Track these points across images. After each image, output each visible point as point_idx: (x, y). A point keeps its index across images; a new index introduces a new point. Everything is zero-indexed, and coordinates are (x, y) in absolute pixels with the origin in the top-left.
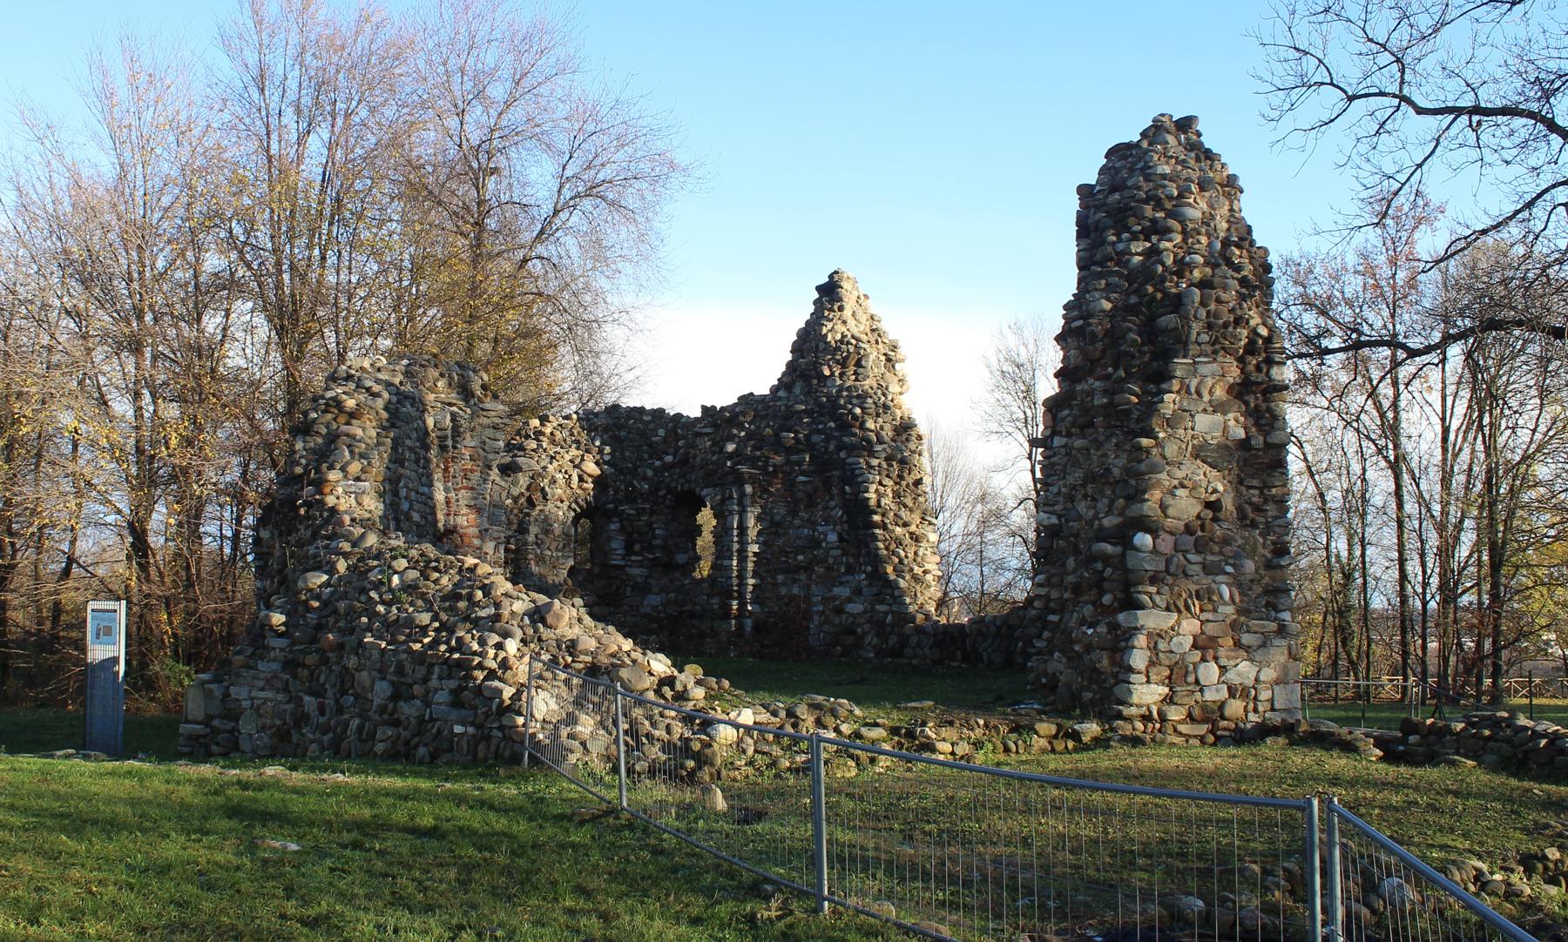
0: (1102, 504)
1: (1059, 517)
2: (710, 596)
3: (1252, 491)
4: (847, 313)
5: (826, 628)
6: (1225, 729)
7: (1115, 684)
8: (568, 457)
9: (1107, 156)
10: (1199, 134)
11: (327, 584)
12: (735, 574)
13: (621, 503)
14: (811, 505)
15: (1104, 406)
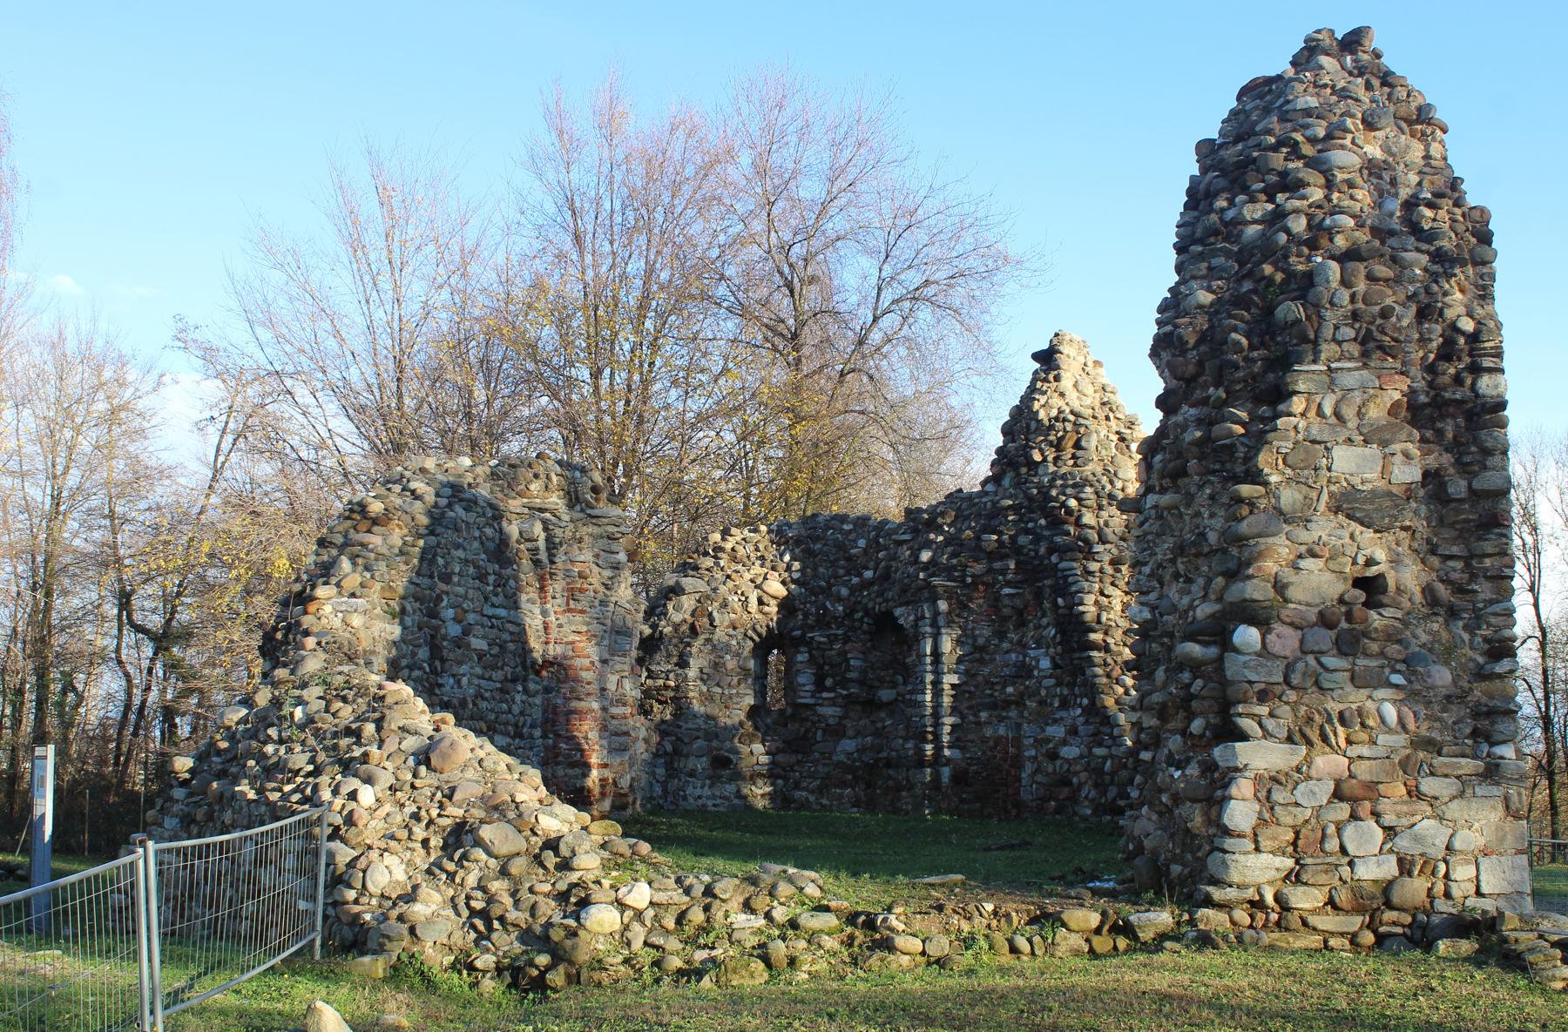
0: (1197, 588)
1: (1153, 608)
2: (906, 739)
3: (1451, 563)
4: (1066, 383)
5: (1039, 778)
6: (1394, 923)
7: (1211, 852)
8: (747, 576)
9: (1239, 98)
10: (1377, 55)
11: (244, 720)
12: (929, 711)
13: (812, 629)
14: (1021, 624)
15: (1198, 443)
